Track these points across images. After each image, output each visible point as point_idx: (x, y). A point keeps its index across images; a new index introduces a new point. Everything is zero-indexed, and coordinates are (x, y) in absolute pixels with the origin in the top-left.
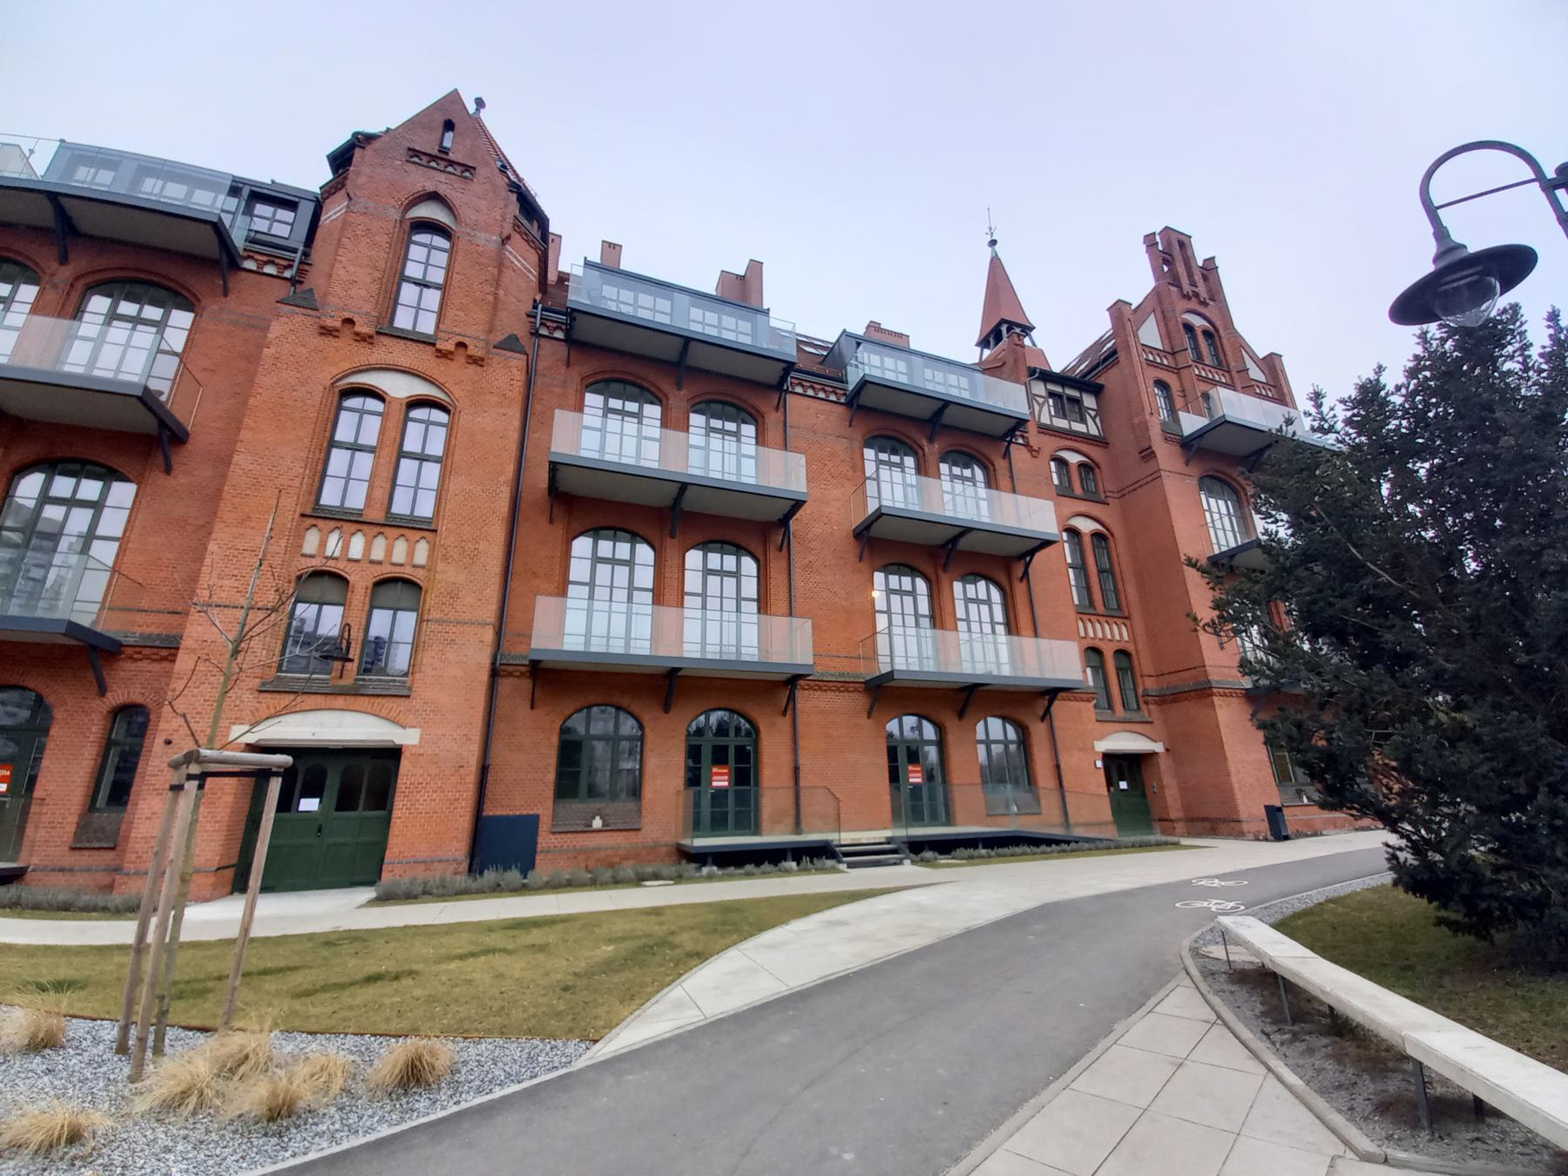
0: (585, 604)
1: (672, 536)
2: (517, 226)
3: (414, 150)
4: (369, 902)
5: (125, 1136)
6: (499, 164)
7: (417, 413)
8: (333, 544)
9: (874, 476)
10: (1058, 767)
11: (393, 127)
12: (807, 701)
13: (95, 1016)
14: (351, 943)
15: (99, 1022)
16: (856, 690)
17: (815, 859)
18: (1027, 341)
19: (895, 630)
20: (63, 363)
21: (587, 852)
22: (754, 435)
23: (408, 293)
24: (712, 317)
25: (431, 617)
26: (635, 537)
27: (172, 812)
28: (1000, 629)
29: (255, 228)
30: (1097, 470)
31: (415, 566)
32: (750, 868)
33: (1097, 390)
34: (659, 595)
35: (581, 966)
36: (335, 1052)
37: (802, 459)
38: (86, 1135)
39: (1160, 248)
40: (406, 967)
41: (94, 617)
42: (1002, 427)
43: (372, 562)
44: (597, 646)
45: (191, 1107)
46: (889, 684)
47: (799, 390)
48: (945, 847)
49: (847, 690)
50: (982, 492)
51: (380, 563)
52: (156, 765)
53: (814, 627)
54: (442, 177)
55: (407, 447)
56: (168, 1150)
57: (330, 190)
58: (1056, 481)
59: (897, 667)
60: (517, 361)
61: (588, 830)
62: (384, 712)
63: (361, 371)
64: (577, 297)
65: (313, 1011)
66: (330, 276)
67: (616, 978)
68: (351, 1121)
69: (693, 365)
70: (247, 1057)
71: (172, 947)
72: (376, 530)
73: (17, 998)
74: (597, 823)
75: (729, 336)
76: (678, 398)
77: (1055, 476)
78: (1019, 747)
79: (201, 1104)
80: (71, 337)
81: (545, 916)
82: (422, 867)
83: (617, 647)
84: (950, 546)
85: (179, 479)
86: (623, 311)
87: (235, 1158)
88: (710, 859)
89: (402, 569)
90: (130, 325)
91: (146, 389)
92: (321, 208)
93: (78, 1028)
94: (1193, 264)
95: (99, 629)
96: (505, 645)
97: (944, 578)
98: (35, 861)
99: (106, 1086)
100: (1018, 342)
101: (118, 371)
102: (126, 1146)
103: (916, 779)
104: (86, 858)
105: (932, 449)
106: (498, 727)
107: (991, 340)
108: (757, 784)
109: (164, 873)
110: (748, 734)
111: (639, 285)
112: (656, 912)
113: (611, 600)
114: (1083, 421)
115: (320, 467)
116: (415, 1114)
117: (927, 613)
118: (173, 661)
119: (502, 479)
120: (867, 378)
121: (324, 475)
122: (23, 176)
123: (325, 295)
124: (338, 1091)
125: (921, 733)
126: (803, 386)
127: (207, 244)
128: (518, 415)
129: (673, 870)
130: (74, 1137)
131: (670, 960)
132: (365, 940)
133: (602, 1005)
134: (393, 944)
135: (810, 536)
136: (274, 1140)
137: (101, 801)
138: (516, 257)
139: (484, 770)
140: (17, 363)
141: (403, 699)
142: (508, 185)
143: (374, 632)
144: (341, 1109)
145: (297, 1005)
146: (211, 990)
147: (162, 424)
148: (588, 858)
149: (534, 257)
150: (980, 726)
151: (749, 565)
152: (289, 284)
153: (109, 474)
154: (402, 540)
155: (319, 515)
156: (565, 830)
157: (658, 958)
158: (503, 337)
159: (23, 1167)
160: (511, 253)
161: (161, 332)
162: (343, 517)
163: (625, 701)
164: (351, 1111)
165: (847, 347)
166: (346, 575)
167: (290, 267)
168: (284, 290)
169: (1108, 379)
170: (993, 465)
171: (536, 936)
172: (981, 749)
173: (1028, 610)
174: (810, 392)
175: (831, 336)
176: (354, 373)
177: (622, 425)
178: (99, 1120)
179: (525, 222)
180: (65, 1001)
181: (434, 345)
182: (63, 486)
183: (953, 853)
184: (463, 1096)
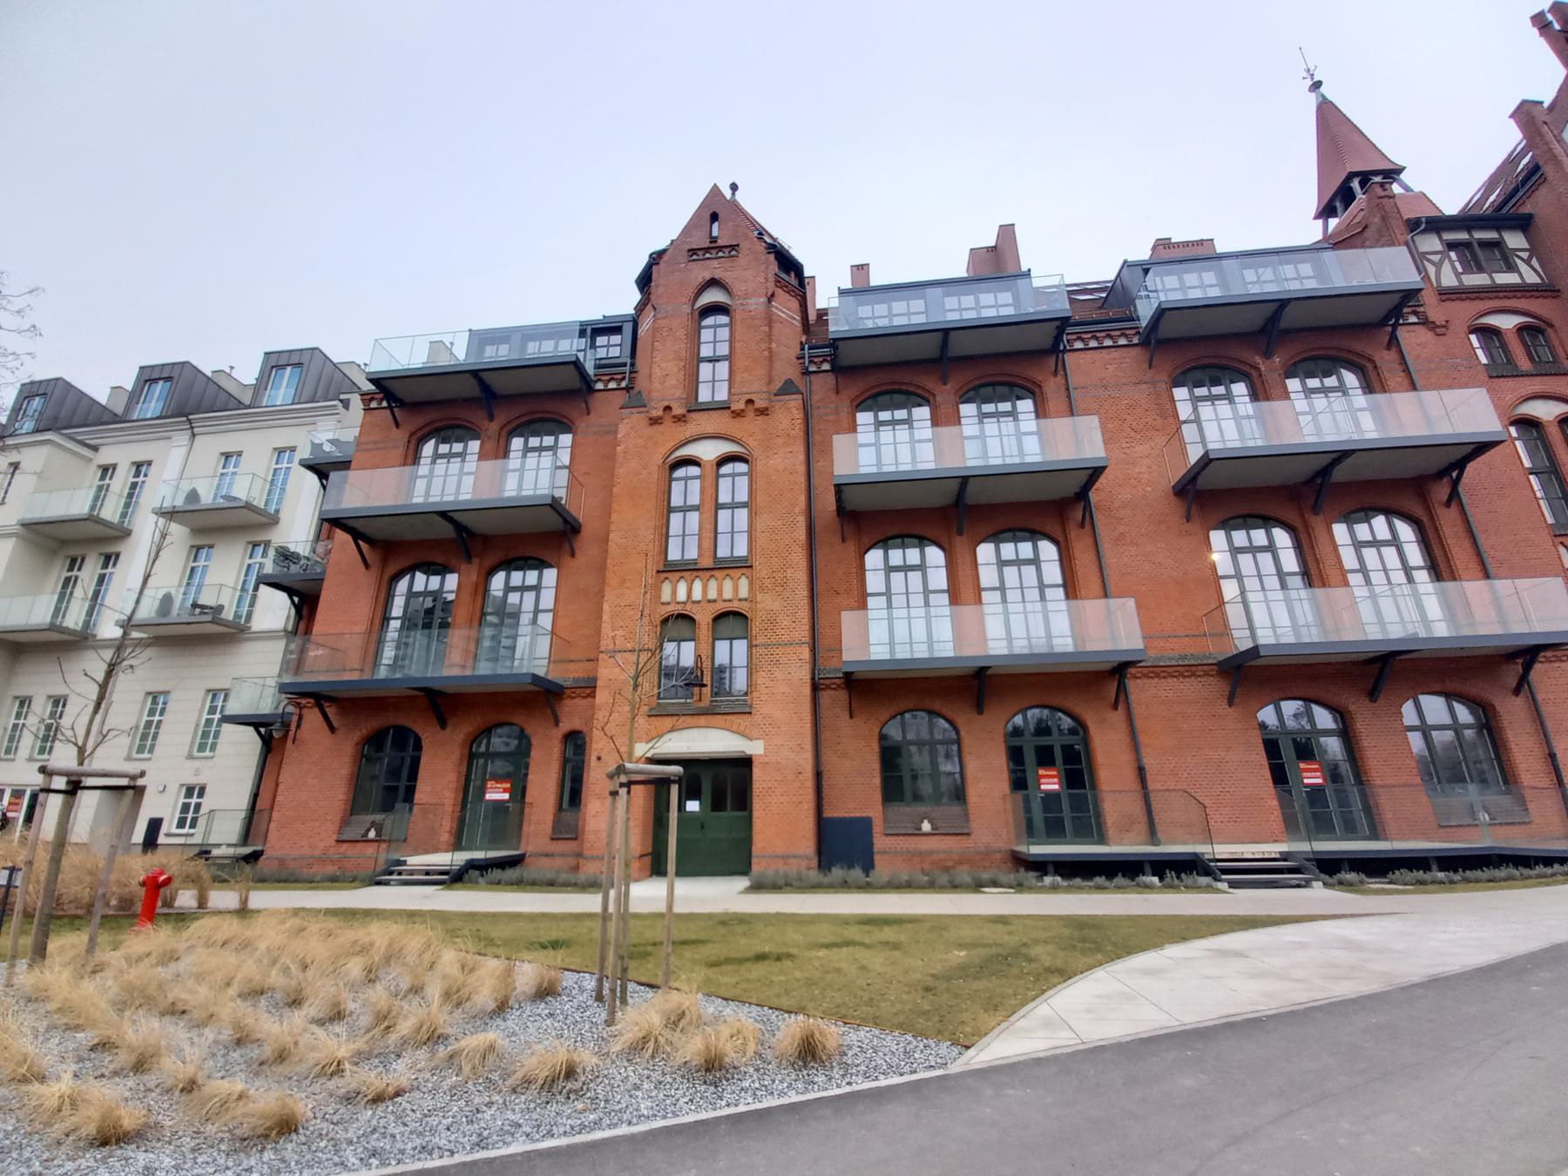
0: (884, 613)
1: (960, 533)
2: (778, 282)
3: (693, 250)
5: (606, 1072)
6: (756, 233)
9: (1192, 417)
10: (1552, 757)
11: (675, 237)
12: (1140, 691)
13: (578, 969)
15: (582, 974)
16: (1206, 674)
17: (1183, 875)
18: (1396, 189)
19: (1251, 597)
20: (504, 491)
21: (920, 854)
22: (1032, 409)
23: (705, 370)
24: (968, 301)
25: (758, 642)
26: (922, 540)
27: (613, 809)
28: (1422, 576)
29: (598, 356)
30: (1549, 330)
31: (740, 600)
32: (1100, 880)
33: (1524, 224)
34: (955, 595)
35: (938, 968)
36: (744, 1018)
37: (1094, 421)
38: (578, 1071)
39: (1557, 27)
40: (784, 950)
41: (545, 669)
42: (1382, 306)
43: (709, 601)
44: (902, 653)
45: (650, 1051)
46: (1253, 663)
47: (1078, 345)
48: (1378, 867)
49: (1193, 675)
50: (1360, 399)
51: (715, 601)
52: (596, 777)
53: (1139, 607)
54: (715, 263)
55: (721, 500)
56: (637, 1087)
57: (641, 307)
58: (1484, 360)
59: (1261, 641)
60: (794, 402)
61: (918, 833)
62: (735, 728)
64: (836, 327)
65: (724, 980)
66: (650, 376)
67: (976, 985)
68: (766, 1083)
69: (955, 355)
70: (684, 1013)
71: (625, 916)
72: (709, 573)
73: (526, 955)
74: (926, 826)
75: (989, 314)
76: (944, 393)
77: (1480, 353)
78: (1480, 733)
79: (656, 1050)
80: (506, 471)
81: (893, 915)
82: (781, 861)
83: (921, 652)
84: (1319, 481)
86: (880, 325)
87: (686, 1100)
88: (1051, 868)
93: (569, 979)
94: (1299, 280)
95: (550, 678)
96: (820, 661)
97: (1317, 522)
98: (530, 849)
99: (591, 1028)
100: (1383, 194)
102: (607, 1082)
103: (1313, 779)
104: (560, 847)
105: (1269, 367)
106: (825, 735)
107: (1338, 204)
108: (1094, 786)
109: (614, 858)
110: (1072, 732)
111: (891, 294)
112: (1002, 920)
113: (908, 606)
114: (1511, 268)
115: (664, 531)
116: (816, 1086)
117: (1296, 569)
118: (594, 697)
119: (797, 510)
120: (1163, 307)
121: (667, 536)
122: (452, 363)
123: (649, 393)
124: (753, 1054)
125: (1311, 720)
126: (1082, 340)
127: (570, 379)
129: (1011, 878)
130: (570, 1072)
131: (1028, 973)
132: (749, 923)
133: (966, 1011)
134: (770, 928)
135: (1116, 505)
136: (712, 1089)
137: (565, 805)
138: (781, 310)
139: (818, 775)
140: (478, 497)
142: (766, 248)
144: (757, 1070)
145: (711, 973)
146: (649, 954)
147: (566, 521)
148: (922, 861)
149: (795, 304)
150: (1408, 709)
151: (1048, 550)
152: (625, 392)
153: (541, 564)
154: (728, 579)
155: (671, 570)
156: (896, 832)
157: (1014, 971)
158: (781, 384)
159: (531, 1101)
160: (777, 308)
163: (937, 705)
164: (765, 1074)
165: (1131, 279)
167: (624, 378)
168: (621, 398)
169: (1539, 204)
170: (1372, 361)
171: (888, 933)
172: (1416, 740)
173: (1467, 544)
174: (1093, 344)
175: (1108, 273)
176: (677, 449)
177: (894, 434)
178: (587, 1058)
179: (784, 276)
180: (559, 957)
181: (729, 408)
182: (517, 577)
183: (1390, 875)
184: (854, 1078)
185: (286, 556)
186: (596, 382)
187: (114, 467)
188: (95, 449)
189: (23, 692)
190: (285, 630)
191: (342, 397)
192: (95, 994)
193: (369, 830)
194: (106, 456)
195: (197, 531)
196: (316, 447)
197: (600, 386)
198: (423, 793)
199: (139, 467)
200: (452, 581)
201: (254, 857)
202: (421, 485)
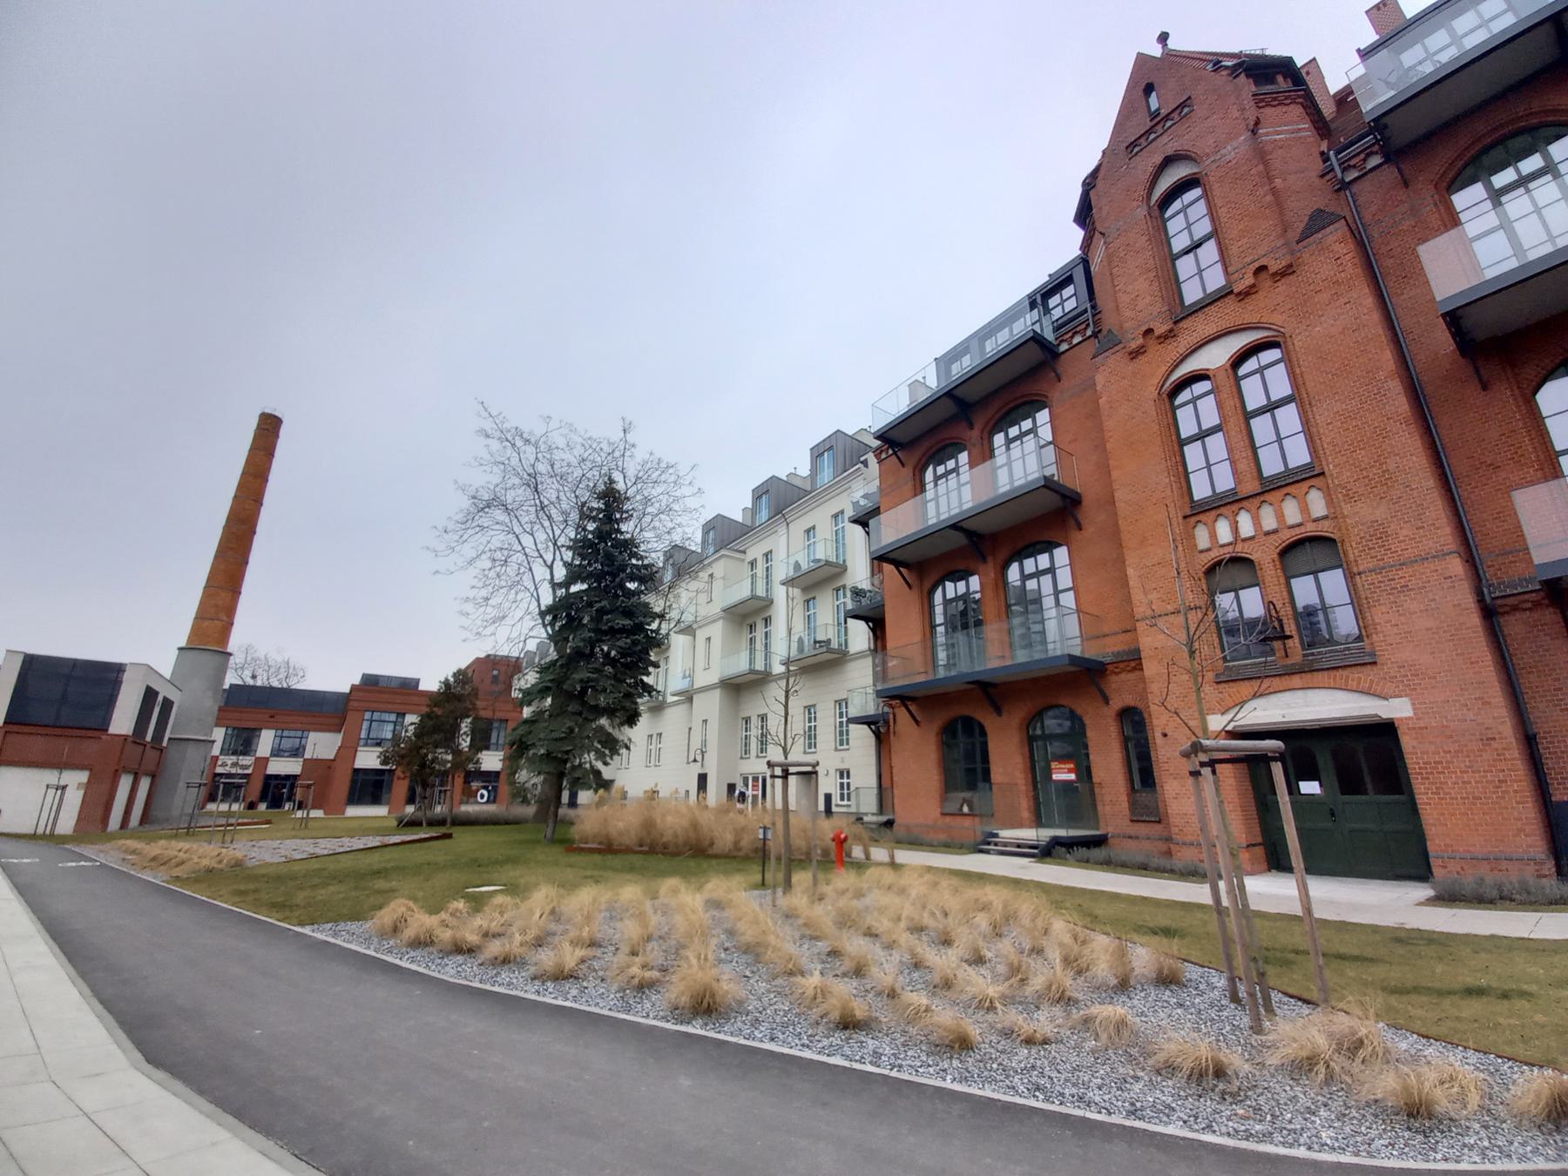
4: (1428, 900)
7: (1244, 369)
8: (1224, 531)
14: (1428, 944)
23: (1185, 266)
31: (1316, 520)
43: (1267, 534)
51: (1275, 532)
52: (1167, 755)
54: (1165, 139)
57: (1086, 245)
63: (1177, 366)
80: (994, 470)
85: (1090, 530)
89: (1302, 529)
90: (1521, 190)
91: (1045, 477)
92: (1088, 262)
96: (1488, 574)
101: (1026, 475)
106: (1527, 682)
119: (1382, 375)
121: (1187, 475)
128: (1366, 290)
139: (1530, 742)
140: (976, 502)
141: (1369, 667)
143: (1300, 603)
147: (1064, 496)
153: (1049, 547)
161: (1036, 435)
162: (1220, 503)
166: (1247, 556)
168: (1092, 345)
176: (1172, 371)
181: (1231, 292)
182: (1029, 565)
185: (857, 593)
186: (1059, 345)
187: (755, 560)
188: (744, 552)
189: (746, 715)
190: (870, 649)
191: (862, 459)
192: (823, 914)
193: (962, 806)
194: (750, 556)
195: (805, 590)
196: (856, 504)
197: (1064, 347)
198: (997, 774)
199: (768, 556)
200: (975, 582)
201: (889, 824)
202: (931, 507)
